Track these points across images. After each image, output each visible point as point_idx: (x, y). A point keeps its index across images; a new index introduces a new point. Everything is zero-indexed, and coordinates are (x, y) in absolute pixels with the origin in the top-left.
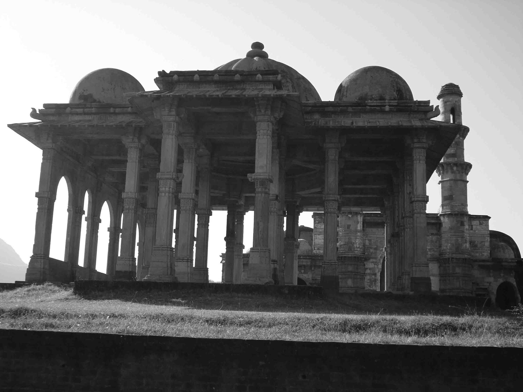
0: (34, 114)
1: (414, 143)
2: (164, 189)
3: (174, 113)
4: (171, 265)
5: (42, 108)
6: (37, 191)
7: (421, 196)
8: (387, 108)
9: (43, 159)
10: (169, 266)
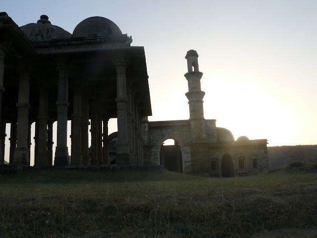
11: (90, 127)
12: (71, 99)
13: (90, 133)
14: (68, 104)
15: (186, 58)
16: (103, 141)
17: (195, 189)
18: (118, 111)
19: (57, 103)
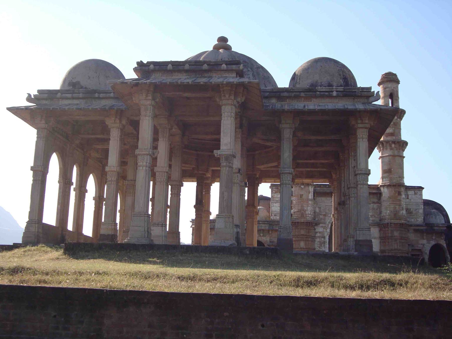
0: (29, 99)
5: (36, 93)
8: (335, 94)
10: (146, 230)
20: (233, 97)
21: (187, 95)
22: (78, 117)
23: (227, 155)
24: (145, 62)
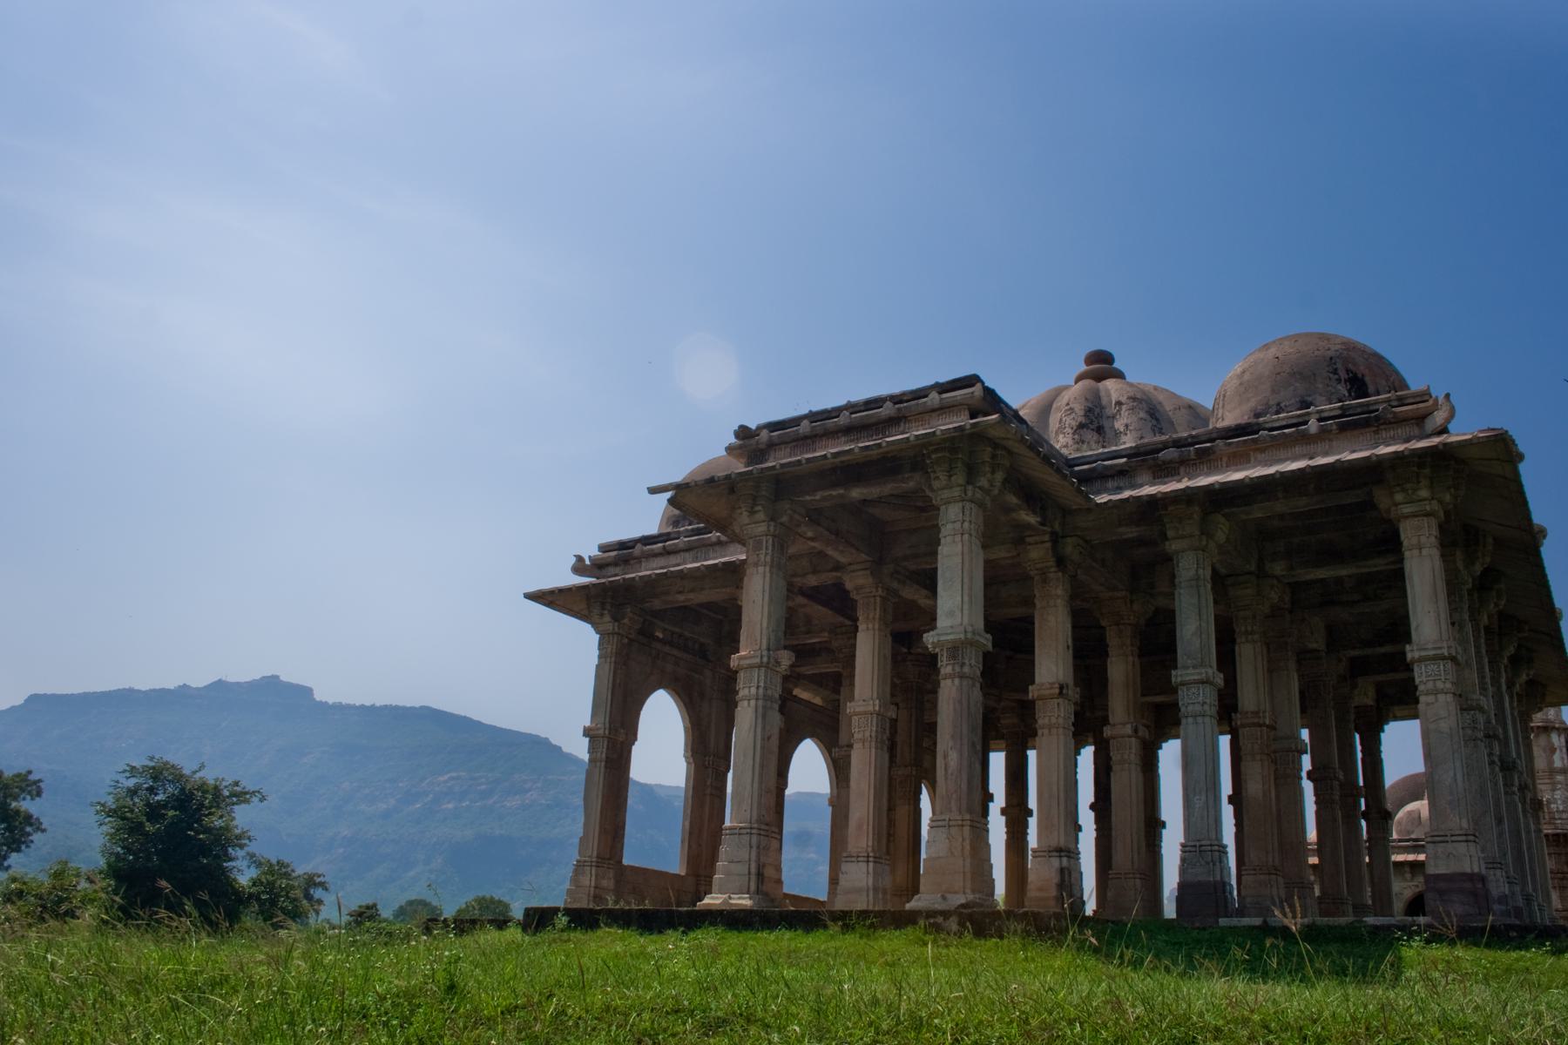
0: (579, 567)
1: (1396, 505)
2: (746, 691)
3: (761, 516)
4: (759, 868)
5: (595, 552)
6: (588, 724)
7: (1430, 646)
8: (1313, 426)
9: (600, 657)
10: (753, 870)
11: (1306, 762)
12: (1226, 659)
13: (1308, 787)
14: (1219, 679)
15: (1542, 532)
16: (1365, 815)
17: (53, 964)
18: (1422, 699)
19: (1177, 676)
20: (959, 478)
21: (856, 493)
22: (681, 598)
23: (954, 641)
24: (753, 426)
